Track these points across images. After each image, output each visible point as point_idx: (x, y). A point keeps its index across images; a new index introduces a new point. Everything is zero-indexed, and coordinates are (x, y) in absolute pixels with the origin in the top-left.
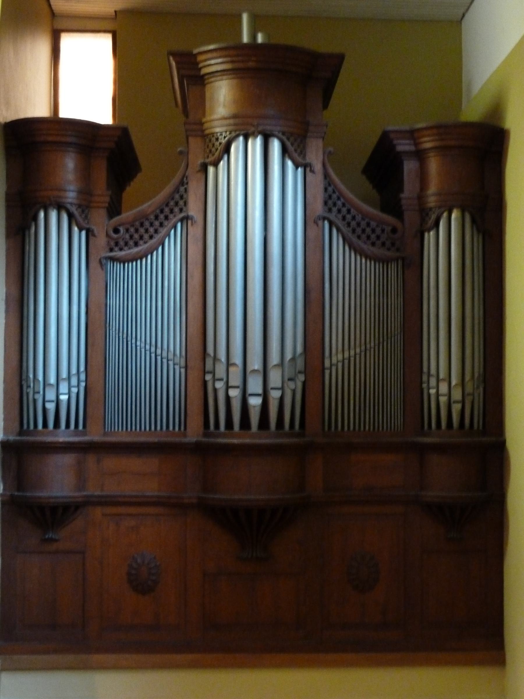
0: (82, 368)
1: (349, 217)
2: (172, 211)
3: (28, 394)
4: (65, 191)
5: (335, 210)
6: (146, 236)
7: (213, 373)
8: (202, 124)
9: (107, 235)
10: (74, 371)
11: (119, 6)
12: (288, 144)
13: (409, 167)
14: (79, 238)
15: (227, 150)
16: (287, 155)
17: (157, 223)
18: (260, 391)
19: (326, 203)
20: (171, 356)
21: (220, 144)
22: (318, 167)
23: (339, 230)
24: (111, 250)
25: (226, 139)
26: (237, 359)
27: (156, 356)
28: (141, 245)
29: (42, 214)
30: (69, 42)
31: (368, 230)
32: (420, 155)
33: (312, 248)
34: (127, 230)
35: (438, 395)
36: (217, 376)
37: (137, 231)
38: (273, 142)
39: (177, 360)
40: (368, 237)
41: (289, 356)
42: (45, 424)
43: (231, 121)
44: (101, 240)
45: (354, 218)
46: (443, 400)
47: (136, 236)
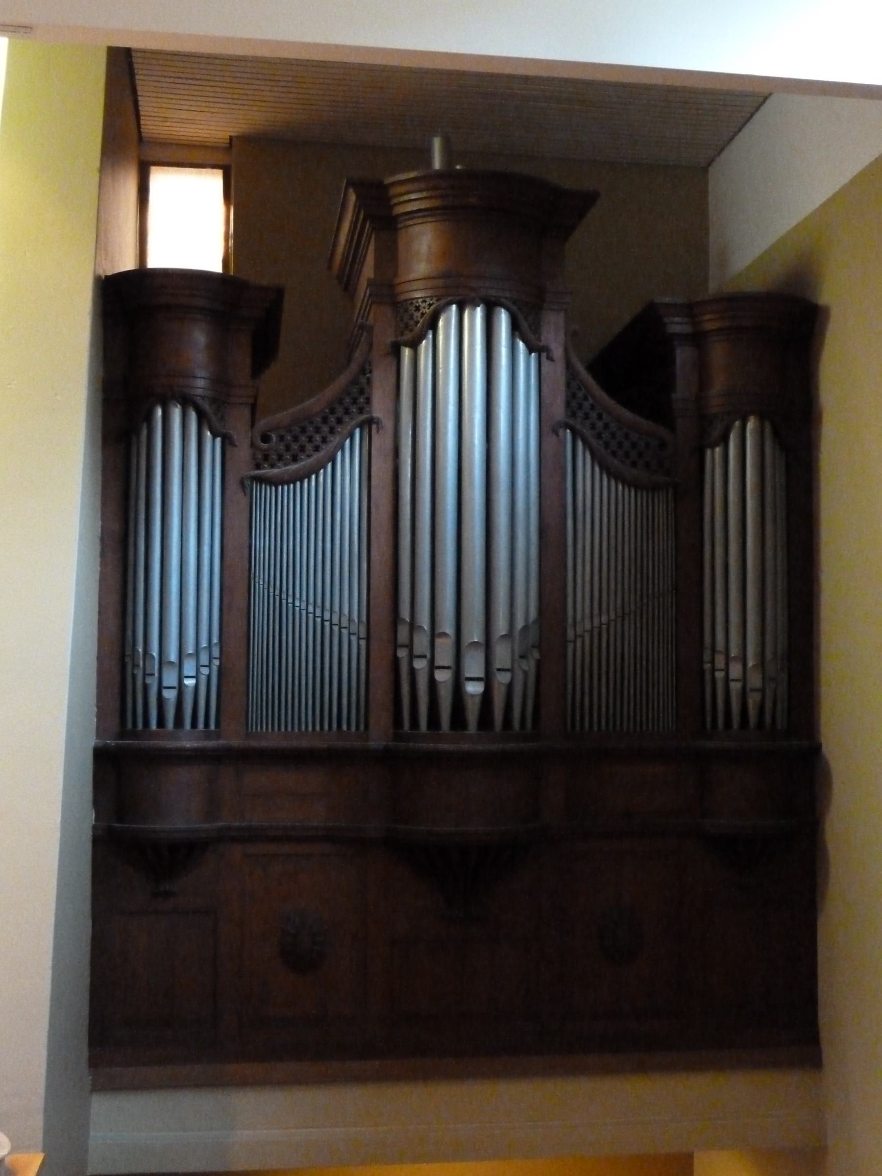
0: (215, 640)
1: (600, 425)
2: (347, 412)
3: (134, 677)
4: (195, 377)
5: (580, 414)
6: (309, 447)
7: (410, 646)
8: (392, 286)
9: (252, 445)
10: (204, 644)
11: (233, 131)
12: (520, 317)
13: (683, 356)
14: (213, 447)
15: (433, 325)
16: (517, 333)
17: (325, 429)
18: (481, 675)
19: (568, 404)
20: (345, 623)
21: (423, 314)
22: (558, 352)
23: (585, 443)
24: (258, 467)
25: (432, 307)
26: (447, 626)
27: (323, 621)
28: (302, 460)
29: (159, 412)
30: (162, 181)
31: (627, 444)
32: (698, 339)
33: (550, 467)
34: (281, 438)
35: (727, 679)
36: (417, 651)
37: (296, 439)
38: (501, 313)
39: (354, 629)
40: (627, 455)
41: (520, 624)
42: (161, 723)
43: (440, 282)
44: (243, 452)
45: (606, 426)
46: (735, 687)
47: (295, 447)
